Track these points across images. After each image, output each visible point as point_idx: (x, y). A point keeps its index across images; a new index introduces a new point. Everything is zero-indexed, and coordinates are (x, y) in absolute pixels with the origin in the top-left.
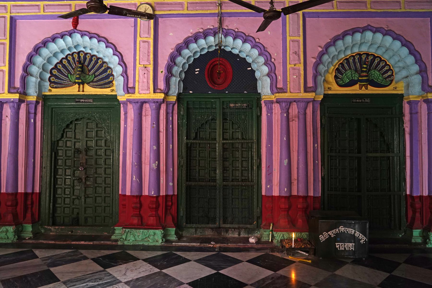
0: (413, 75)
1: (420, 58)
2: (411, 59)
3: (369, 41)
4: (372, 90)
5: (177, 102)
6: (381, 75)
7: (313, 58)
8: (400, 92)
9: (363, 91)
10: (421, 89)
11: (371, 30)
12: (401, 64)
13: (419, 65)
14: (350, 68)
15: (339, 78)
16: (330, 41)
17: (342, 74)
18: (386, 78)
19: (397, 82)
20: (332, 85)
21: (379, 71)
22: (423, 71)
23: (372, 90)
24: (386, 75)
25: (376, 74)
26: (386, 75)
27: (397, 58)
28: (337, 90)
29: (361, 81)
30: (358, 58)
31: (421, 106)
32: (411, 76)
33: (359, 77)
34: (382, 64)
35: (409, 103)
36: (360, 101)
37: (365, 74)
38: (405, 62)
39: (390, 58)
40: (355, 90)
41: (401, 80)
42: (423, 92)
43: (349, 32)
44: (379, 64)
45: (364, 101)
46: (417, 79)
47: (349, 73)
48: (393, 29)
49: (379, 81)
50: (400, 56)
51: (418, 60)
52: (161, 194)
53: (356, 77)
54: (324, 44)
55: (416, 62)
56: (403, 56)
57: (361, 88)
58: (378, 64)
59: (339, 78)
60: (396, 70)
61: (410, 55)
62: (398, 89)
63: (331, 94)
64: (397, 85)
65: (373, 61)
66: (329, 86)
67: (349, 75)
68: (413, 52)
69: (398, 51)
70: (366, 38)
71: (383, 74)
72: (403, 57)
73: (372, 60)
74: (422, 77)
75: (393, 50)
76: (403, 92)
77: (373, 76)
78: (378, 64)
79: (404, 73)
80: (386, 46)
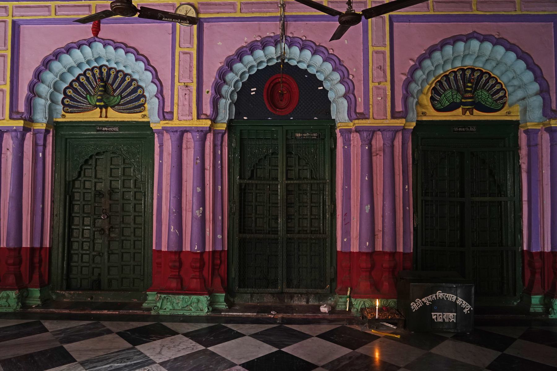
0: (532, 96)
2: (529, 76)
3: (475, 53)
4: (479, 116)
6: (491, 97)
7: (402, 74)
8: (514, 119)
9: (468, 117)
11: (477, 39)
15: (437, 100)
18: (496, 101)
19: (510, 106)
20: (427, 109)
21: (488, 91)
22: (544, 92)
23: (479, 116)
24: (497, 96)
25: (483, 95)
26: (497, 96)
28: (434, 115)
29: (465, 104)
33: (462, 99)
35: (527, 132)
36: (464, 129)
37: (469, 95)
38: (522, 80)
40: (457, 115)
41: (516, 103)
43: (448, 41)
45: (468, 130)
46: (537, 101)
47: (449, 93)
49: (488, 104)
50: (515, 72)
51: (539, 77)
53: (458, 98)
55: (536, 80)
56: (518, 72)
57: (464, 113)
59: (437, 100)
60: (510, 89)
62: (512, 114)
64: (510, 110)
66: (424, 110)
69: (511, 65)
73: (478, 76)
74: (544, 98)
75: (506, 64)
76: (519, 118)
79: (520, 94)
80: (496, 59)
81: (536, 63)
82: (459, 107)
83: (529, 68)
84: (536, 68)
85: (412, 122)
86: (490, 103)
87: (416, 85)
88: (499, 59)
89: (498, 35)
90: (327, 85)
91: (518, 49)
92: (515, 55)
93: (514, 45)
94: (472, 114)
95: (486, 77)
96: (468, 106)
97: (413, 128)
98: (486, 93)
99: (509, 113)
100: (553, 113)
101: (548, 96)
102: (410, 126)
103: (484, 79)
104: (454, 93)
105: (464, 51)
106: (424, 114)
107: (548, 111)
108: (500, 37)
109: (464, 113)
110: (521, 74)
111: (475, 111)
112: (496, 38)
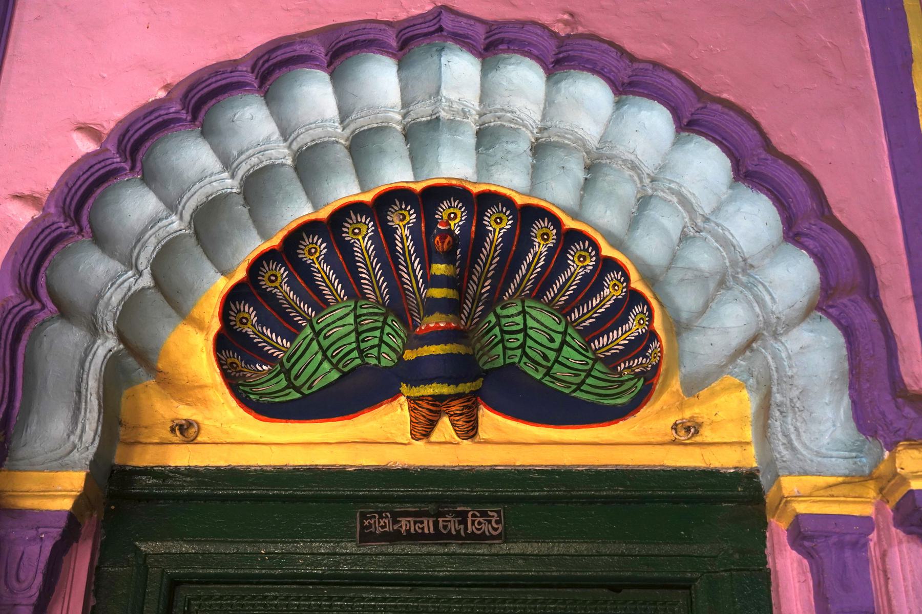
0: (790, 326)
1: (810, 203)
2: (753, 220)
3: (465, 114)
4: (509, 443)
5: (89, 525)
6: (578, 342)
7: (19, 197)
8: (725, 459)
9: (446, 450)
10: (856, 432)
11: (464, 41)
12: (703, 258)
13: (812, 254)
14: (355, 292)
15: (269, 359)
16: (162, 94)
17: (290, 330)
18: (611, 362)
19: (694, 387)
20: (205, 403)
21: (564, 311)
22: (848, 291)
23: (509, 443)
24: (619, 338)
25: (533, 330)
26: (619, 338)
27: (667, 221)
28: (237, 438)
29: (415, 373)
30: (414, 230)
31: (884, 555)
32: (775, 335)
33: (406, 346)
34: (579, 265)
35: (805, 534)
36: (428, 526)
37: (437, 321)
38: (727, 243)
39: (634, 222)
40: (381, 438)
41: (719, 371)
42: (872, 446)
43: (305, 50)
44: (598, 287)
45: (453, 526)
46: (816, 351)
47: (340, 320)
48: (608, 28)
49: (562, 379)
50: (684, 201)
51: (806, 217)
52: (896, 549)
53: (388, 347)
54: (120, 115)
55: (793, 233)
56: (705, 205)
57: (423, 429)
58: (557, 261)
59: (269, 359)
60: (687, 300)
61: (790, 247)
62: (707, 435)
63: (192, 472)
64: (695, 411)
65: (517, 241)
66: (185, 413)
67: (343, 325)
68: (756, 164)
69: (662, 168)
70: (444, 92)
71: (590, 334)
72: (707, 211)
73: (508, 236)
74: (848, 332)
75: (634, 167)
76: (749, 459)
77: (515, 342)
78: (557, 261)
79: (733, 319)
80: (583, 142)
81: (786, 150)
82: (394, 394)
83: (689, 124)
84: (784, 175)
85: (64, 467)
86: (576, 372)
87: (115, 266)
88: (593, 143)
89: (566, 23)
90: (616, 545)
91: (676, 81)
92: (714, 150)
93: (656, 65)
94: (470, 431)
95: (545, 237)
96: (428, 381)
97: (67, 504)
98: (548, 320)
99: (691, 428)
100: (909, 411)
101: (872, 316)
102: (45, 494)
103: (540, 247)
104: (367, 323)
105: (406, 104)
106: (185, 430)
107: (884, 405)
108: (581, 30)
109: (423, 429)
110: (717, 210)
111: (489, 419)
112: (554, 35)
